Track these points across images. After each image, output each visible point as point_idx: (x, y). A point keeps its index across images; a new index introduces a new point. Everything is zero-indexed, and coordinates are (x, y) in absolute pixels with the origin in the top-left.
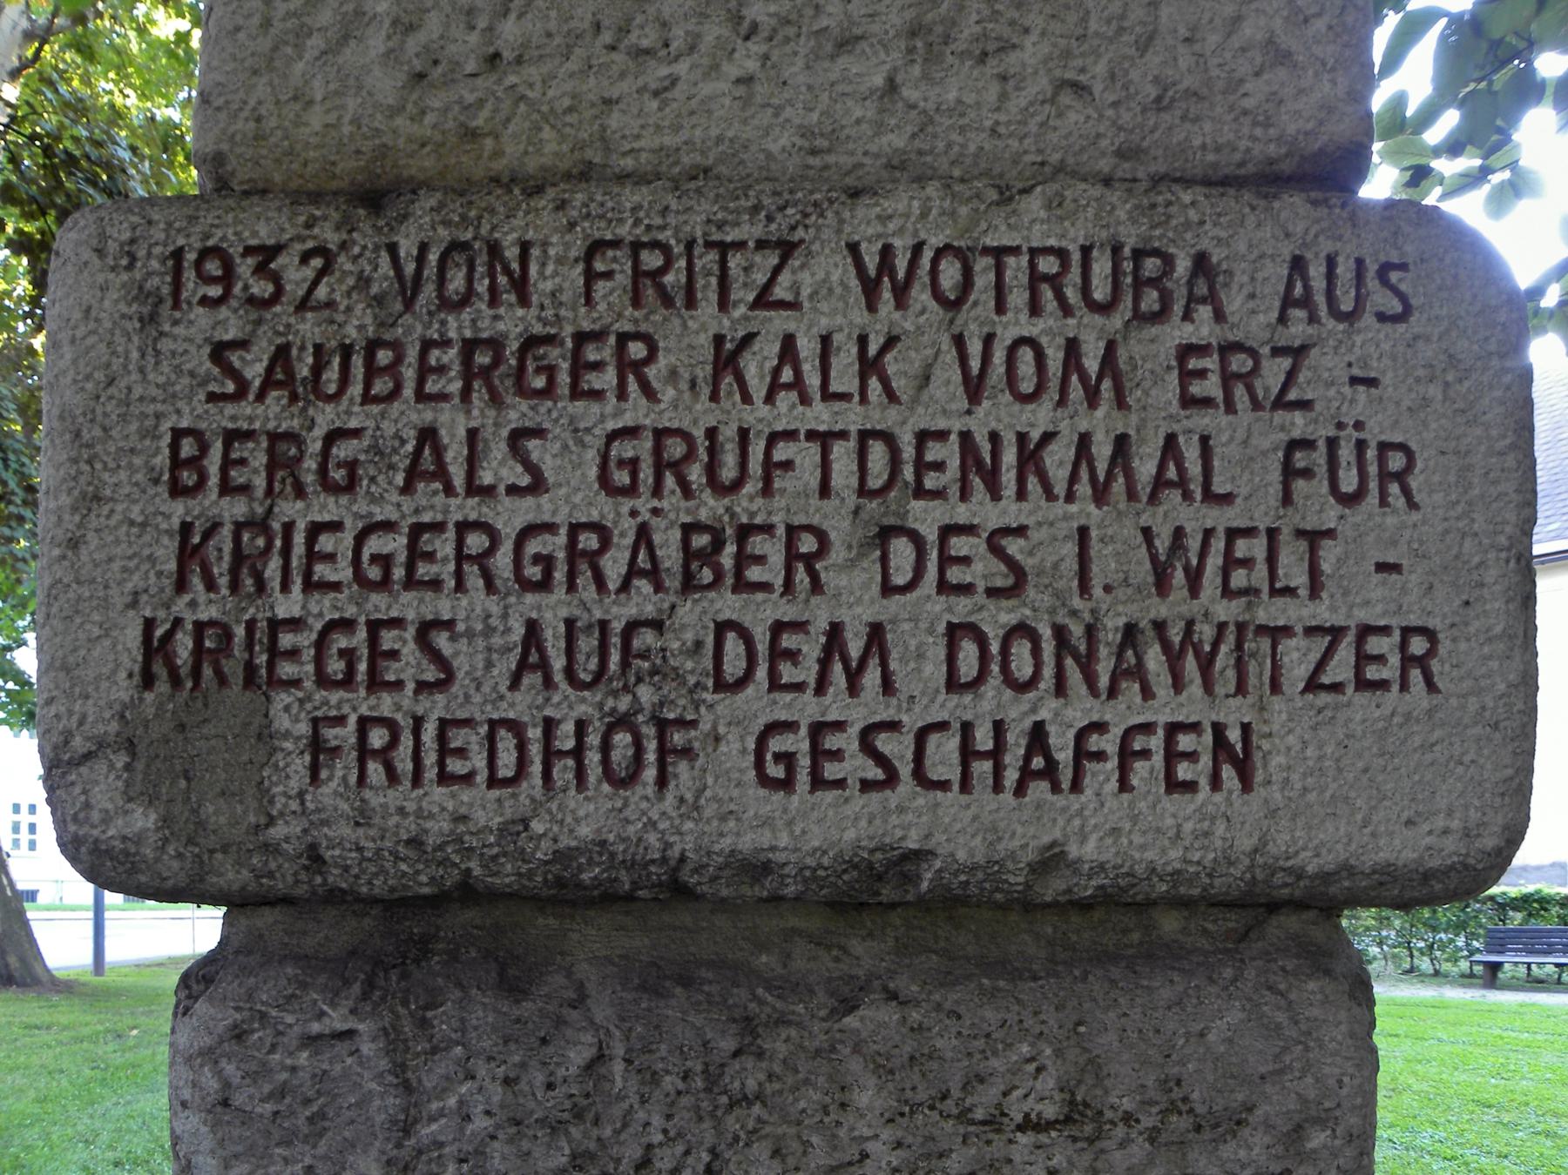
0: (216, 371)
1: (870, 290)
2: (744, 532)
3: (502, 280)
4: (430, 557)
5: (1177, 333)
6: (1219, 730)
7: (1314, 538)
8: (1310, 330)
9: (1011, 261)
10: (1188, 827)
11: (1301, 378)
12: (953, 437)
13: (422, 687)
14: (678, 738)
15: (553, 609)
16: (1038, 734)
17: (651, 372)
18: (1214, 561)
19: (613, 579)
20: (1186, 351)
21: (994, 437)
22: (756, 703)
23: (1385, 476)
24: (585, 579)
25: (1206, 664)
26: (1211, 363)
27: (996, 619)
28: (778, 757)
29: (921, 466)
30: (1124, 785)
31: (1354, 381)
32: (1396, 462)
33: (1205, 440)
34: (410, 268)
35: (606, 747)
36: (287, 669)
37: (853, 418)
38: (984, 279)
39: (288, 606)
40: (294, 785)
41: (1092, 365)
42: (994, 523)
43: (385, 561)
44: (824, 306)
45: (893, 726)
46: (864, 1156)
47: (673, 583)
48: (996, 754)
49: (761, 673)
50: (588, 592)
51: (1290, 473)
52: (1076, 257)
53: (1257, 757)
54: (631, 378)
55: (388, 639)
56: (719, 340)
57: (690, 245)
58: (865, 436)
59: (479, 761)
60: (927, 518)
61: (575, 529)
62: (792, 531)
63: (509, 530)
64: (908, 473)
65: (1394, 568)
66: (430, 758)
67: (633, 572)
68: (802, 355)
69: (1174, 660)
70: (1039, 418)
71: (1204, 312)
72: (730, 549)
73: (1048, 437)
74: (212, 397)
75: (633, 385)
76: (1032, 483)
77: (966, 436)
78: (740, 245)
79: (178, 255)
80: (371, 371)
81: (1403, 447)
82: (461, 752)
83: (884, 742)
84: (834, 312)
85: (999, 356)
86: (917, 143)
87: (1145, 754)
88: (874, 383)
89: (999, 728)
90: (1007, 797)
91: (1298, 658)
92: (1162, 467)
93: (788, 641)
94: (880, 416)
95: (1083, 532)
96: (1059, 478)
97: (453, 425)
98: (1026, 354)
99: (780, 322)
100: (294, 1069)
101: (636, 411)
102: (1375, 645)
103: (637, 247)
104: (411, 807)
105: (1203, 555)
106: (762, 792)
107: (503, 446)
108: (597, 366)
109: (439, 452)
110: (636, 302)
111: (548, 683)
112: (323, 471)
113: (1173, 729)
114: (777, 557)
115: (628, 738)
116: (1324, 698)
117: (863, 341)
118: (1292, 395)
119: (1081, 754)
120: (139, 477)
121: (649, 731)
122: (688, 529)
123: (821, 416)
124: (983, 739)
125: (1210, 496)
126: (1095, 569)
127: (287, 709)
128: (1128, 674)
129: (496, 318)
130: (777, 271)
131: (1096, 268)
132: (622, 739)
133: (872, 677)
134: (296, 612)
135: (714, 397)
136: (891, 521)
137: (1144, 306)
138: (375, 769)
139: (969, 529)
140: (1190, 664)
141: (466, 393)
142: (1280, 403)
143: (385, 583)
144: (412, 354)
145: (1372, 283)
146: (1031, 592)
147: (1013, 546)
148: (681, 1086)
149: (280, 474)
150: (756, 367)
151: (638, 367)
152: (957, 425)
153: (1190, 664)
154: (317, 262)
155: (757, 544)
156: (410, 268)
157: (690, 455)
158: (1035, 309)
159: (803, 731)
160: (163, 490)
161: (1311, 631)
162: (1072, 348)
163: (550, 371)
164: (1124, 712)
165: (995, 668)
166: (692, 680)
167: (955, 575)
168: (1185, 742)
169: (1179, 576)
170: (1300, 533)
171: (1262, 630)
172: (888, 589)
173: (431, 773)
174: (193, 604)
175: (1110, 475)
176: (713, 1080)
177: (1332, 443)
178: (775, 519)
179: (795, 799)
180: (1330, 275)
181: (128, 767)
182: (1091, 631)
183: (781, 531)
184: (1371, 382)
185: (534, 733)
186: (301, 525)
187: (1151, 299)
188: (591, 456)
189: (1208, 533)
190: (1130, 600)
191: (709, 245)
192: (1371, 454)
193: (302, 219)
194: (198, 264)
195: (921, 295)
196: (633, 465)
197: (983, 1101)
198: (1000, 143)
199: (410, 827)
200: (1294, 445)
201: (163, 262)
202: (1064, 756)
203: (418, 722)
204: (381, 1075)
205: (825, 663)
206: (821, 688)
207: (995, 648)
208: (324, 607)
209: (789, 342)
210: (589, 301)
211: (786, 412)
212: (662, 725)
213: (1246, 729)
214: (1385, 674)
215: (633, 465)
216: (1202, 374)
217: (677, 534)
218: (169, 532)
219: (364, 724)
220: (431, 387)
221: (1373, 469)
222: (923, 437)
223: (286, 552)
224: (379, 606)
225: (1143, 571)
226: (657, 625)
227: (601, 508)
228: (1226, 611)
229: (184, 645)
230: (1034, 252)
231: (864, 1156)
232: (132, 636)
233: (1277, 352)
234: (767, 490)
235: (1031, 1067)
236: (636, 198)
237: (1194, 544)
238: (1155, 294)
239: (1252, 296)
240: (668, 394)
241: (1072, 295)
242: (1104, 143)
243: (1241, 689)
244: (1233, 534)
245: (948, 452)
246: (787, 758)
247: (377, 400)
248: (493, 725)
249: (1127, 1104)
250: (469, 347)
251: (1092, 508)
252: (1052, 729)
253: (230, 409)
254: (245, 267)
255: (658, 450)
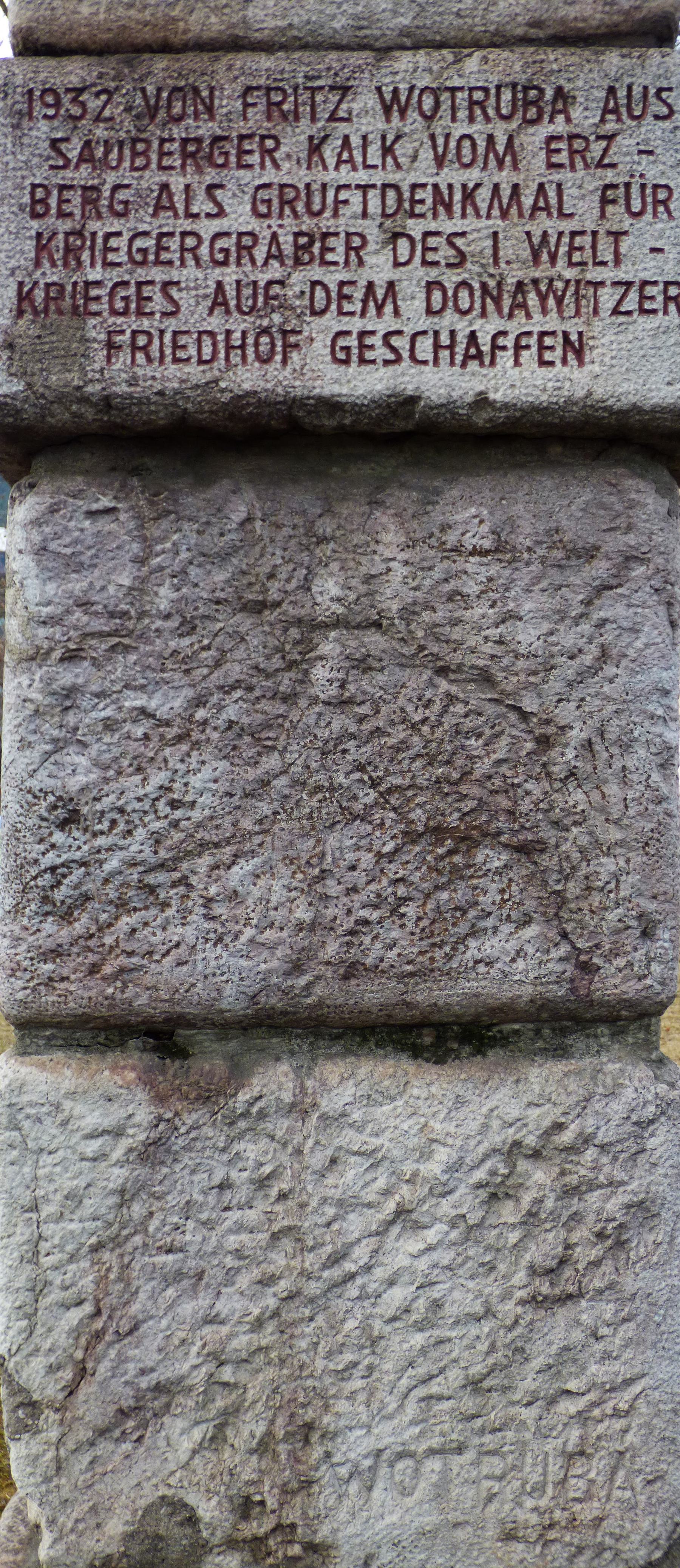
0: (53, 154)
1: (387, 110)
2: (325, 236)
3: (201, 107)
4: (167, 249)
5: (545, 130)
6: (566, 335)
7: (617, 235)
8: (617, 126)
9: (459, 95)
10: (550, 384)
11: (611, 152)
12: (429, 188)
13: (165, 314)
14: (292, 339)
15: (230, 275)
16: (473, 336)
17: (277, 155)
18: (563, 249)
19: (260, 261)
20: (551, 139)
21: (450, 186)
22: (331, 322)
23: (656, 202)
24: (245, 260)
25: (559, 301)
26: (563, 145)
27: (450, 279)
28: (342, 348)
29: (413, 202)
30: (517, 363)
31: (640, 152)
32: (662, 195)
33: (559, 186)
34: (152, 102)
35: (257, 344)
36: (94, 307)
37: (378, 178)
38: (446, 106)
39: (95, 274)
40: (97, 366)
41: (500, 149)
42: (449, 231)
43: (144, 251)
44: (364, 121)
45: (399, 333)
46: (389, 570)
47: (289, 262)
48: (451, 347)
49: (334, 307)
50: (248, 268)
51: (605, 201)
52: (493, 91)
53: (586, 348)
54: (267, 159)
55: (147, 291)
56: (311, 138)
57: (296, 88)
58: (385, 186)
59: (193, 351)
60: (416, 228)
61: (240, 235)
62: (348, 235)
63: (206, 237)
64: (407, 205)
65: (660, 250)
66: (168, 351)
67: (269, 256)
68: (353, 145)
69: (543, 298)
70: (474, 175)
71: (560, 118)
72: (318, 245)
73: (478, 186)
74: (52, 167)
75: (268, 162)
76: (470, 210)
77: (436, 186)
78: (321, 88)
79: (30, 92)
80: (135, 154)
81: (666, 187)
82: (184, 347)
83: (395, 341)
84: (369, 124)
85: (453, 144)
86: (416, 22)
87: (528, 347)
88: (389, 160)
89: (453, 334)
90: (457, 368)
91: (608, 298)
92: (536, 201)
93: (346, 290)
94: (394, 177)
95: (495, 234)
96: (483, 206)
97: (177, 183)
98: (467, 143)
99: (343, 128)
100: (82, 530)
101: (270, 176)
102: (650, 291)
103: (269, 89)
104: (158, 375)
105: (558, 245)
106: (335, 366)
107: (203, 193)
108: (250, 152)
109: (170, 196)
110: (269, 118)
111: (228, 312)
112: (111, 207)
113: (543, 334)
114: (341, 249)
115: (267, 340)
116: (622, 319)
117: (384, 138)
118: (606, 161)
119: (495, 347)
120: (14, 209)
121: (278, 336)
122: (297, 235)
123: (362, 176)
124: (445, 340)
125: (562, 215)
126: (501, 253)
127: (95, 327)
128: (519, 306)
129: (198, 127)
130: (340, 102)
131: (503, 97)
132: (264, 339)
133: (389, 308)
134: (98, 277)
135: (309, 168)
136: (398, 230)
137: (528, 116)
138: (140, 357)
139: (437, 234)
140: (551, 302)
141: (183, 166)
142: (600, 165)
143: (144, 263)
144: (155, 145)
145: (652, 99)
146: (469, 265)
147: (459, 242)
148: (292, 533)
149: (88, 208)
150: (329, 153)
151: (270, 152)
152: (431, 181)
153: (551, 302)
154: (104, 97)
155: (332, 242)
156: (152, 102)
157: (297, 198)
158: (471, 119)
159: (355, 335)
160: (27, 216)
161: (616, 284)
162: (491, 139)
163: (226, 154)
164: (514, 327)
165: (451, 304)
166: (299, 311)
167: (431, 256)
168: (548, 341)
169: (545, 257)
170: (609, 233)
171: (589, 283)
172: (397, 264)
173: (169, 359)
174: (44, 274)
175: (509, 205)
176: (309, 531)
177: (628, 185)
178: (340, 229)
179: (351, 370)
180: (629, 96)
181: (10, 358)
182: (499, 284)
183: (343, 235)
184: (650, 153)
185: (221, 338)
186: (100, 234)
187: (532, 113)
188: (247, 198)
189: (561, 234)
190: (519, 269)
191: (306, 88)
192: (649, 191)
193: (95, 74)
194: (42, 97)
195: (413, 115)
196: (269, 202)
197: (451, 538)
198: (461, 21)
199: (158, 386)
200: (607, 187)
201: (23, 95)
202: (486, 349)
203: (162, 332)
204: (131, 531)
205: (365, 302)
206: (363, 314)
207: (450, 293)
208: (115, 275)
209: (346, 138)
210: (245, 118)
211: (345, 175)
212: (285, 333)
213: (580, 334)
214: (654, 306)
215: (269, 202)
216: (558, 151)
217: (290, 238)
218: (30, 238)
219: (134, 333)
220: (166, 162)
221: (649, 199)
222: (414, 187)
223: (92, 248)
224: (142, 274)
225: (527, 254)
226: (281, 283)
227: (253, 225)
228: (570, 274)
229: (39, 295)
230: (471, 89)
231: (389, 570)
232: (12, 292)
233: (599, 138)
234: (336, 214)
235: (477, 521)
236: (268, 64)
237: (553, 240)
238: (534, 110)
239: (586, 109)
240: (286, 166)
241: (491, 112)
242: (520, 19)
243: (578, 313)
244: (574, 234)
245: (426, 195)
246: (347, 349)
247: (137, 169)
248: (200, 333)
249: (528, 543)
250: (185, 141)
251: (499, 222)
252: (478, 334)
253: (62, 173)
254: (66, 99)
255: (281, 195)
